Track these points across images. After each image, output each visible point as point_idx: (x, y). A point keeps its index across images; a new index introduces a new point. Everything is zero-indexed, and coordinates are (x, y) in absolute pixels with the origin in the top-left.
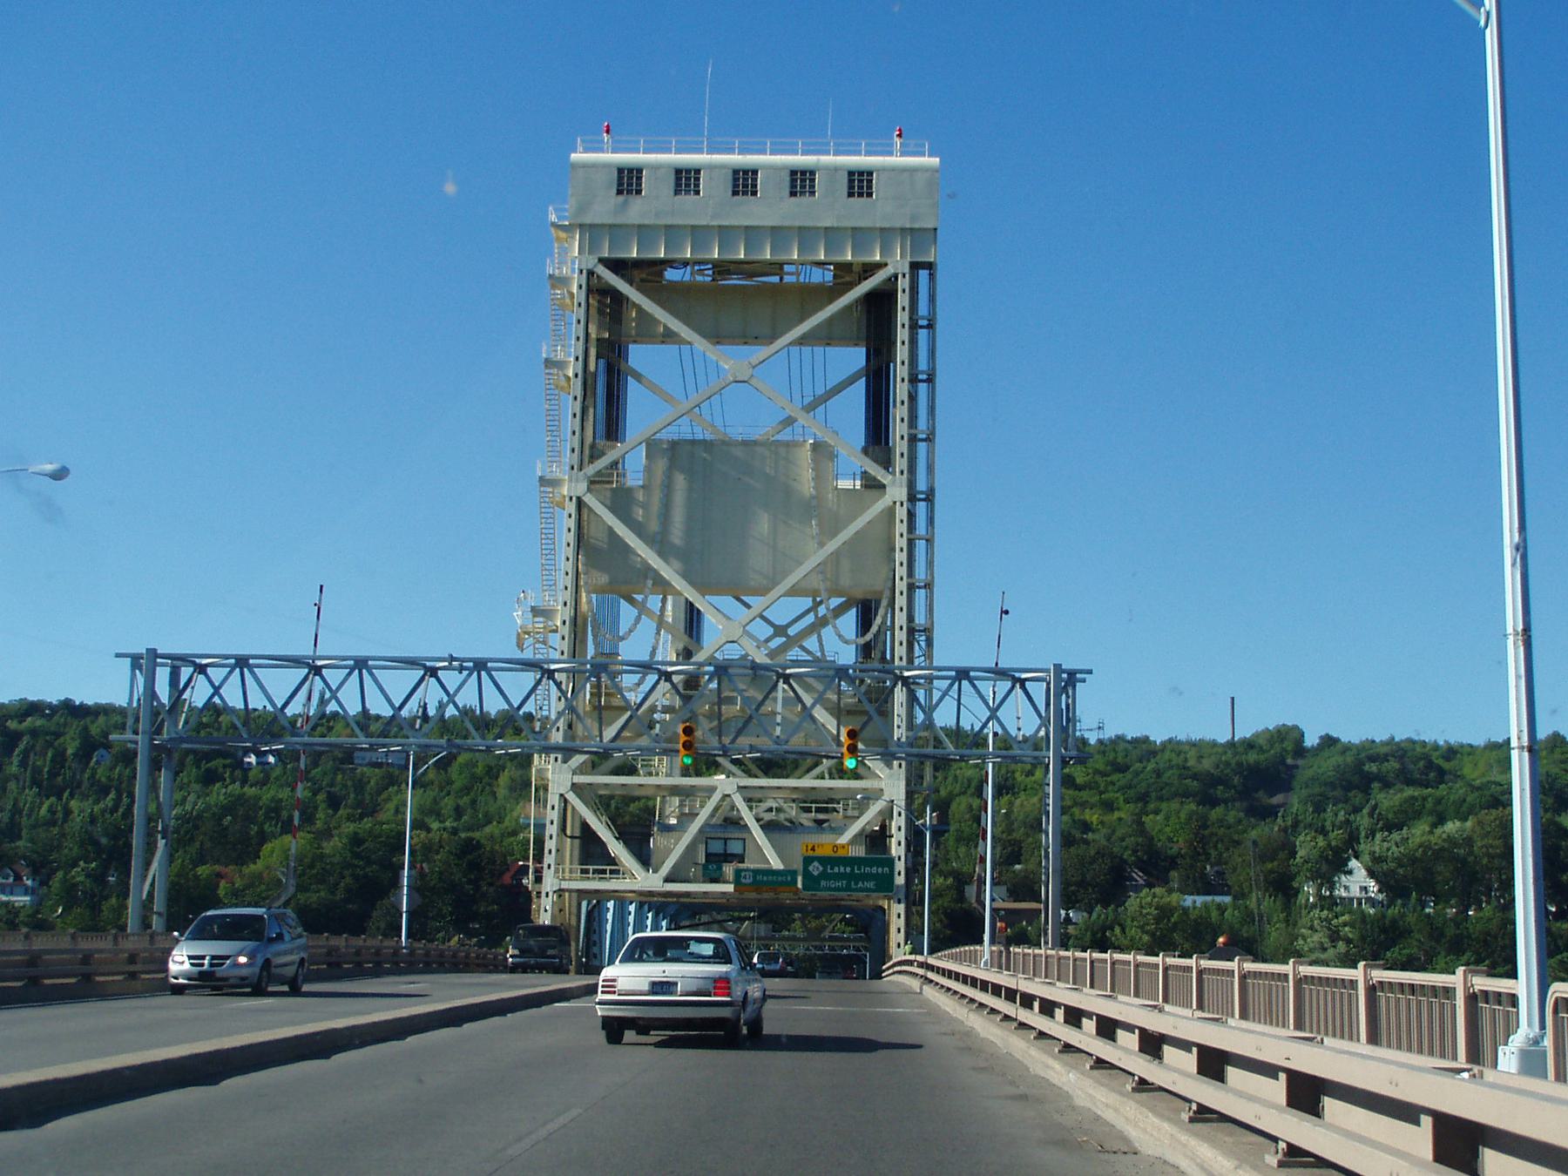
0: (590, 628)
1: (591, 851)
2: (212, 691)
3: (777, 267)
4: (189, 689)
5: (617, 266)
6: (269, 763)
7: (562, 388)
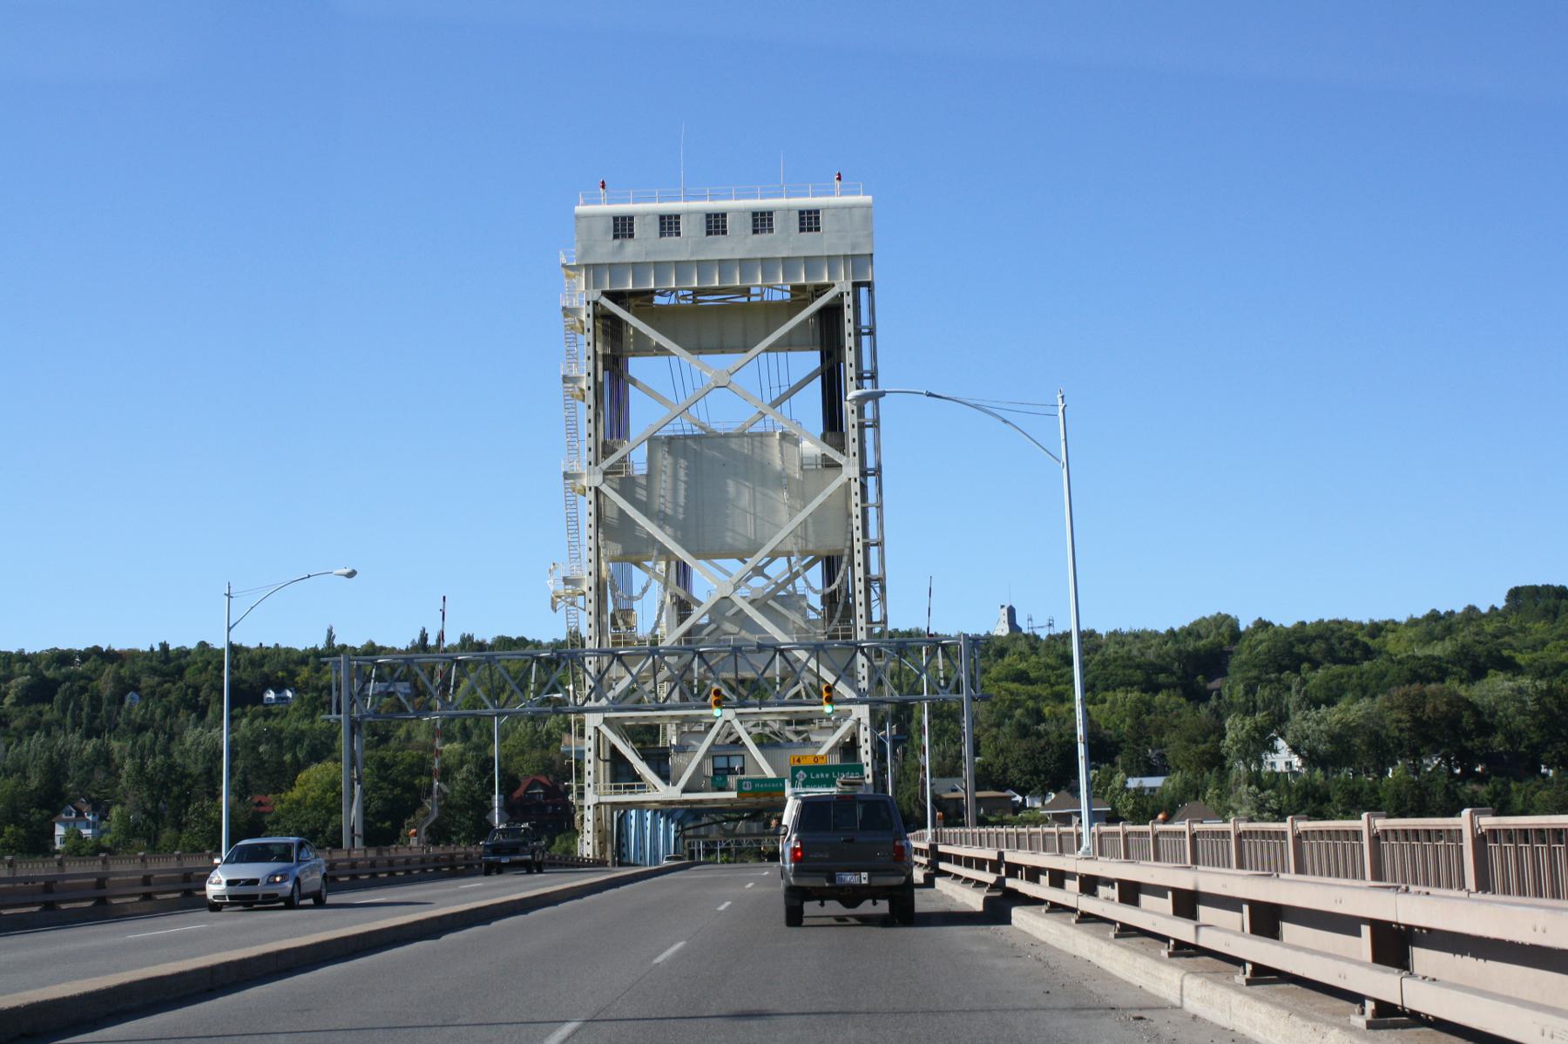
0: (609, 591)
1: (620, 771)
3: (746, 291)
5: (616, 297)
6: (287, 698)
7: (577, 397)
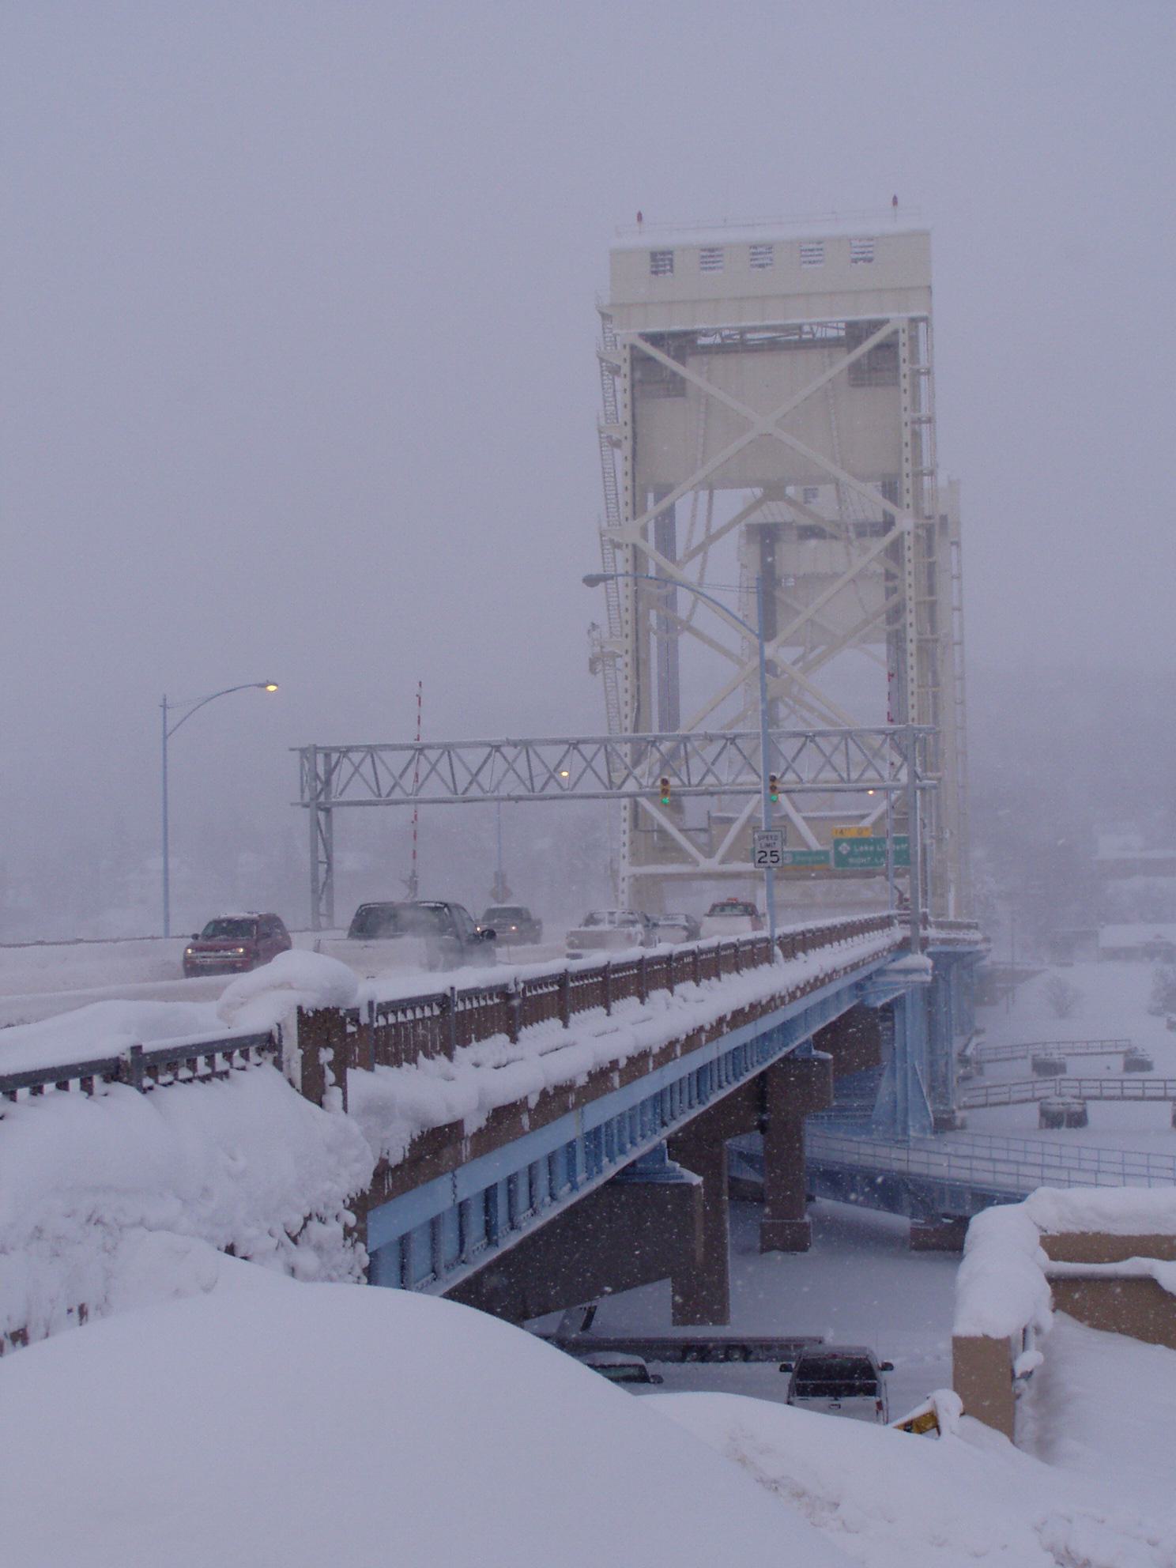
4: (338, 767)
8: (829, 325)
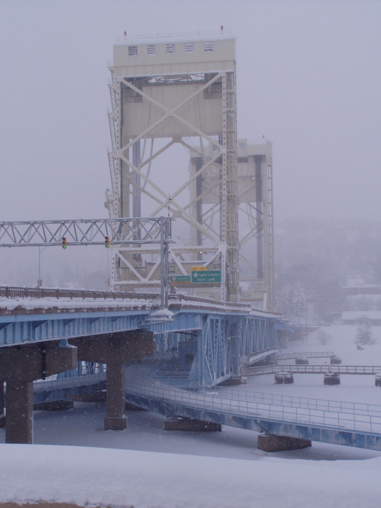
2: (69, 229)
8: (199, 75)
